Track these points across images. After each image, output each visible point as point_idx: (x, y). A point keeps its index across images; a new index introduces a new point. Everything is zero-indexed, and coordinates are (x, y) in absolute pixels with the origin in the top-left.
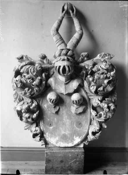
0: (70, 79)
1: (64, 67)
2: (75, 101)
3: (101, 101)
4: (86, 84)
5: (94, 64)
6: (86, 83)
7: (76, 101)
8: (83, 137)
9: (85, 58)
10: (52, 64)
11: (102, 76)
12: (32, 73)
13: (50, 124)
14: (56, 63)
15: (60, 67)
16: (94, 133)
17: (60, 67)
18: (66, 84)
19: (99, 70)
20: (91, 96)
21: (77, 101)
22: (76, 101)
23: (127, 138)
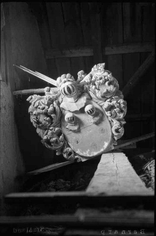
0: (79, 97)
1: (68, 88)
2: (89, 112)
3: (111, 102)
4: (92, 95)
5: (91, 77)
6: (91, 93)
7: (90, 110)
8: (110, 139)
9: (83, 76)
10: (58, 92)
11: (101, 81)
12: (44, 104)
13: (78, 142)
14: (103, 156)
15: (64, 88)
16: (117, 131)
17: (64, 88)
18: (76, 102)
19: (97, 77)
20: (100, 103)
21: (91, 110)
22: (90, 110)
23: (148, 234)
